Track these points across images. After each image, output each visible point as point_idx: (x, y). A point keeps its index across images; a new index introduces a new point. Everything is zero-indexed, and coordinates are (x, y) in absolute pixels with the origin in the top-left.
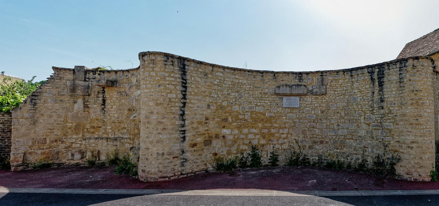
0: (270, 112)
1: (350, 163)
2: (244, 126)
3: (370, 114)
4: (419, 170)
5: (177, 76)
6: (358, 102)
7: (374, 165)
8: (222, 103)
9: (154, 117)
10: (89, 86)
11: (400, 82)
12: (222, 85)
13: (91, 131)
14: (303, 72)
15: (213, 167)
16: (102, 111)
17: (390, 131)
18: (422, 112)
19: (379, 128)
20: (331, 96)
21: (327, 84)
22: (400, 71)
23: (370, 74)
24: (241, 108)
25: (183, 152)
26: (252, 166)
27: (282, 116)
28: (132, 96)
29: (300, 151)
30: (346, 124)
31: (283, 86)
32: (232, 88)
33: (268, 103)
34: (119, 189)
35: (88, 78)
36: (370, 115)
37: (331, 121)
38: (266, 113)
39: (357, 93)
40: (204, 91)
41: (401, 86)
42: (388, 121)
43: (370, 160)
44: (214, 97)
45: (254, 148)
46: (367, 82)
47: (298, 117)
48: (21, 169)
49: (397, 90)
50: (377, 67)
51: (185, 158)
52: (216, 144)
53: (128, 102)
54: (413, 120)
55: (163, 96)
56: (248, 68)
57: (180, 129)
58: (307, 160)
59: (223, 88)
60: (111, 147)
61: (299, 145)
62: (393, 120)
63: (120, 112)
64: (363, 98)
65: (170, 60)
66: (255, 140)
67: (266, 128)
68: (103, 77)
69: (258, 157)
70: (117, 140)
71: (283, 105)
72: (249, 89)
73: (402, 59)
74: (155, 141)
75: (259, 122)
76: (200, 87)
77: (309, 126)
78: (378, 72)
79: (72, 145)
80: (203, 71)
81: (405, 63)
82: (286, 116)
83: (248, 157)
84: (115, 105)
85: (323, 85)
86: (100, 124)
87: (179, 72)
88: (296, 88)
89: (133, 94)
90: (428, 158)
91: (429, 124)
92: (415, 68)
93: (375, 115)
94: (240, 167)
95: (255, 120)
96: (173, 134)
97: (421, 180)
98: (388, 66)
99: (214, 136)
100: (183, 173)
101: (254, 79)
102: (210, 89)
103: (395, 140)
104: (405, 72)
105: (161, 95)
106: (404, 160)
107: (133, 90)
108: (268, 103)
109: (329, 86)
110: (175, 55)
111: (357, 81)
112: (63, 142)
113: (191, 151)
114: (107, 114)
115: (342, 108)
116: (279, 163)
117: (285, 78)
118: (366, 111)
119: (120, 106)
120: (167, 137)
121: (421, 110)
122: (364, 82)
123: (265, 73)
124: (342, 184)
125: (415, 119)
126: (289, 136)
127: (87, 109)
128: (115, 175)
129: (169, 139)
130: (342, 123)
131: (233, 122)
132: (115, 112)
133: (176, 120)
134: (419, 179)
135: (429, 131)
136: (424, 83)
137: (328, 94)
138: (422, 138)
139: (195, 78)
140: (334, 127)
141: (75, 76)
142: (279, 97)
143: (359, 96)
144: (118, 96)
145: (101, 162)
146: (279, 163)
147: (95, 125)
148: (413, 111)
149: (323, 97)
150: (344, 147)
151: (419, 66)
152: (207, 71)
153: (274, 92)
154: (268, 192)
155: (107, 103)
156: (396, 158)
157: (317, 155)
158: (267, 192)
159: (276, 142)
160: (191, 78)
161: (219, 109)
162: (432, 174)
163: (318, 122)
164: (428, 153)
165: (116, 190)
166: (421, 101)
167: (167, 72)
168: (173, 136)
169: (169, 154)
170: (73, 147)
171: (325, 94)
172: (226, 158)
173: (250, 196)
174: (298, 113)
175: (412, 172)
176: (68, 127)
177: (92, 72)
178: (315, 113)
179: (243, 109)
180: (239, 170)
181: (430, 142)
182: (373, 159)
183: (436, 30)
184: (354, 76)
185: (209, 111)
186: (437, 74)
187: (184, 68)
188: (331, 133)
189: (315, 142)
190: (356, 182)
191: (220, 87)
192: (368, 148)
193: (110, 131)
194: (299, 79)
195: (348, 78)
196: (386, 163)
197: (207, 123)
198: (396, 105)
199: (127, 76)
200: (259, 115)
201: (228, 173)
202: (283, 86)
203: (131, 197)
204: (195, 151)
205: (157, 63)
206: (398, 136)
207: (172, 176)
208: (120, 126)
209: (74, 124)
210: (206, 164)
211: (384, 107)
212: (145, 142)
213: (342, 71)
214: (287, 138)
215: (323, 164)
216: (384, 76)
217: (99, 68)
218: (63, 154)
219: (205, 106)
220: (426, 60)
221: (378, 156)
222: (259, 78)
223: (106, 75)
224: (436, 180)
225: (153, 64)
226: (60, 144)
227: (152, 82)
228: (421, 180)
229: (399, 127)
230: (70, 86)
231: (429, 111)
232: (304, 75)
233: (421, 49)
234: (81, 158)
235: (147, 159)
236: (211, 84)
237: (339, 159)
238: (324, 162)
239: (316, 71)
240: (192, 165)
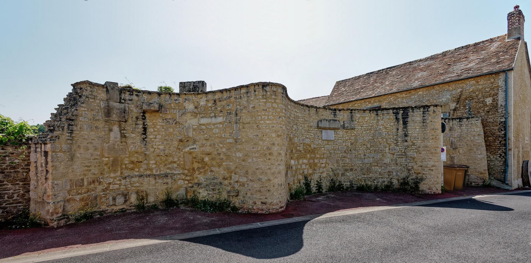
1: (377, 185)
4: (437, 186)
6: (383, 136)
10: (125, 110)
11: (423, 122)
13: (130, 167)
17: (414, 158)
19: (403, 156)
20: (359, 131)
21: (356, 120)
22: (423, 114)
23: (395, 114)
35: (123, 100)
42: (412, 151)
48: (64, 224)
49: (420, 128)
54: (433, 150)
70: (167, 176)
71: (322, 138)
78: (403, 113)
79: (110, 187)
81: (428, 109)
86: (141, 158)
103: (418, 165)
104: (428, 115)
109: (357, 122)
111: (382, 120)
112: (100, 183)
114: (149, 146)
118: (391, 143)
126: (327, 165)
132: (160, 143)
137: (356, 129)
140: (361, 157)
141: (109, 96)
144: (163, 124)
147: (134, 159)
150: (370, 173)
155: (149, 132)
170: (111, 188)
176: (104, 162)
189: (346, 170)
193: (154, 166)
194: (334, 114)
206: (421, 162)
209: (111, 159)
211: (408, 140)
214: (325, 167)
216: (408, 117)
218: (101, 198)
225: (275, 95)
226: (97, 186)
227: (274, 114)
230: (104, 108)
235: (269, 191)
237: (367, 183)
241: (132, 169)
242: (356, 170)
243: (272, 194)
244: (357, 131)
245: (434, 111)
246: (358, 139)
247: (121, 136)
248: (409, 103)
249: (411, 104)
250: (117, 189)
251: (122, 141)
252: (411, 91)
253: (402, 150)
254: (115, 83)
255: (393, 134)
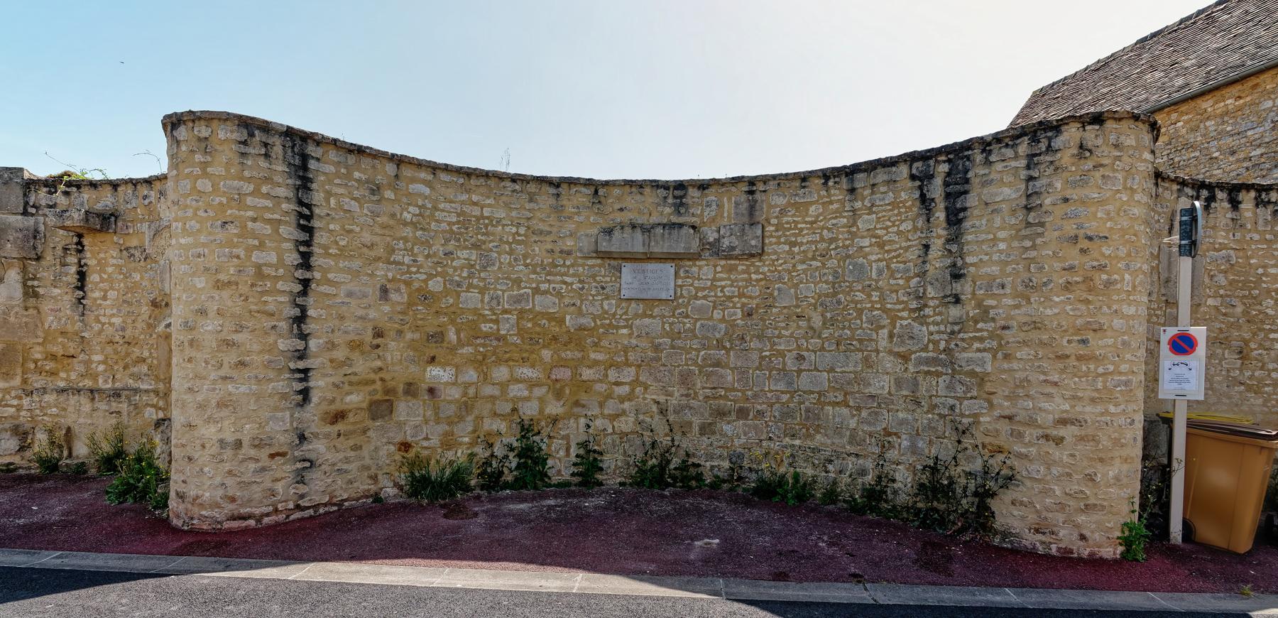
0: (580, 313)
1: (835, 483)
2: (497, 357)
3: (910, 321)
4: (1081, 519)
5: (282, 192)
6: (871, 279)
7: (916, 495)
8: (425, 281)
9: (210, 325)
10: (36, 231)
11: (1026, 207)
12: (429, 224)
13: (48, 368)
14: (688, 181)
15: (396, 485)
16: (77, 307)
17: (982, 379)
18: (1104, 314)
19: (940, 368)
20: (780, 262)
21: (768, 220)
22: (1028, 167)
23: (918, 183)
24: (487, 298)
25: (302, 438)
26: (519, 484)
27: (618, 328)
28: (162, 262)
29: (673, 440)
30: (827, 354)
31: (622, 228)
32: (461, 234)
33: (572, 284)
34: (102, 552)
35: (33, 206)
36: (913, 323)
37: (775, 344)
38: (568, 317)
39: (867, 249)
40: (369, 244)
41: (1031, 220)
42: (976, 345)
43: (904, 479)
44: (403, 264)
45: (526, 429)
46: (906, 212)
47: (668, 329)
50: (943, 158)
51: (308, 456)
52: (408, 414)
53: (152, 280)
54: (1069, 342)
55: (238, 257)
56: (512, 170)
57: (292, 365)
58: (693, 471)
59: (432, 234)
60: (104, 417)
61: (668, 421)
62: (995, 343)
63: (129, 312)
64: (888, 267)
65: (258, 139)
66: (529, 404)
67: (563, 363)
68: (78, 201)
69: (537, 457)
71: (620, 291)
72: (514, 238)
73: (1040, 123)
74: (214, 403)
75: (544, 347)
76: (358, 229)
77: (704, 359)
78: (949, 174)
80: (367, 177)
82: (631, 327)
83: (506, 457)
84: (114, 290)
85: (752, 225)
87: (290, 181)
88: (663, 234)
89: (163, 254)
90: (1117, 479)
91: (1128, 356)
92: (1088, 154)
93: (928, 324)
94: (483, 487)
95: (531, 339)
96: (270, 380)
97: (1085, 553)
98: (983, 151)
99: (401, 388)
100: (303, 503)
101: (532, 205)
102: (388, 238)
103: (997, 413)
104: (1050, 171)
105: (232, 256)
106: (1028, 483)
107: (163, 242)
108: (572, 284)
110: (275, 123)
113: (327, 436)
114: (90, 317)
115: (813, 301)
116: (605, 477)
117: (631, 201)
118: (899, 311)
119: (127, 293)
120: (251, 389)
121: (1101, 307)
122: (896, 212)
123: (565, 186)
124: (808, 558)
125: (1076, 338)
127: (32, 301)
128: (106, 506)
129: (258, 397)
130: (813, 351)
131: (461, 344)
132: (115, 311)
133: (280, 336)
134: (1078, 549)
135: (1127, 383)
136: (1120, 210)
137: (769, 254)
138: (1099, 409)
139: (341, 199)
140: (784, 364)
142: (609, 264)
143: (875, 261)
144: (121, 262)
145: (75, 462)
146: (605, 477)
148: (1071, 310)
149: (750, 265)
151: (1104, 148)
152: (379, 177)
153: (592, 248)
154: (560, 579)
156: (998, 473)
157: (726, 454)
158: (557, 579)
159: (596, 411)
160: (328, 201)
161: (418, 301)
162: (1127, 533)
163: (731, 348)
164: (1117, 461)
165: (93, 555)
166: (1104, 277)
167: (249, 180)
168: (270, 387)
169: (258, 444)
171: (761, 255)
172: (438, 457)
173: (497, 591)
174: (670, 317)
175: (1055, 526)
177: (46, 186)
178: (724, 315)
179: (495, 302)
180: (478, 497)
181: (1129, 421)
182: (915, 474)
183: (1147, 37)
184: (860, 190)
185: (387, 308)
186: (1159, 180)
187: (304, 167)
188: (775, 385)
190: (854, 553)
191: (421, 232)
192: (899, 437)
193: (101, 368)
194: (674, 205)
195: (841, 197)
196: (959, 491)
197: (378, 346)
198: (1008, 291)
199: (145, 197)
200: (544, 321)
201: (443, 506)
202: (622, 228)
203: (128, 580)
204: (339, 435)
205: (216, 150)
206: (1007, 398)
207: (268, 515)
208: (128, 354)
210: (376, 477)
211: (963, 297)
212: (184, 406)
213: (820, 174)
214: (630, 397)
215: (744, 483)
216: (966, 187)
217: (67, 174)
219: (373, 292)
220: (1131, 123)
221: (935, 464)
222: (548, 203)
223: (86, 195)
224: (1141, 556)
227: (201, 213)
228: (1086, 553)
229: (1015, 365)
231: (1132, 310)
232: (693, 192)
233: (1086, 105)
234: (19, 450)
235: (190, 459)
236: (392, 222)
237: (798, 470)
238: (746, 477)
239: (733, 178)
240: (329, 481)
241: (53, 373)
242: (760, 414)
243: (198, 469)
244: (773, 261)
245: (1081, 147)
246: (776, 293)
247: (26, 294)
248: (1249, 133)
249: (1256, 136)
250: (11, 417)
251: (28, 305)
252: (1262, 77)
253: (938, 342)
254: (15, 168)
255: (908, 270)
